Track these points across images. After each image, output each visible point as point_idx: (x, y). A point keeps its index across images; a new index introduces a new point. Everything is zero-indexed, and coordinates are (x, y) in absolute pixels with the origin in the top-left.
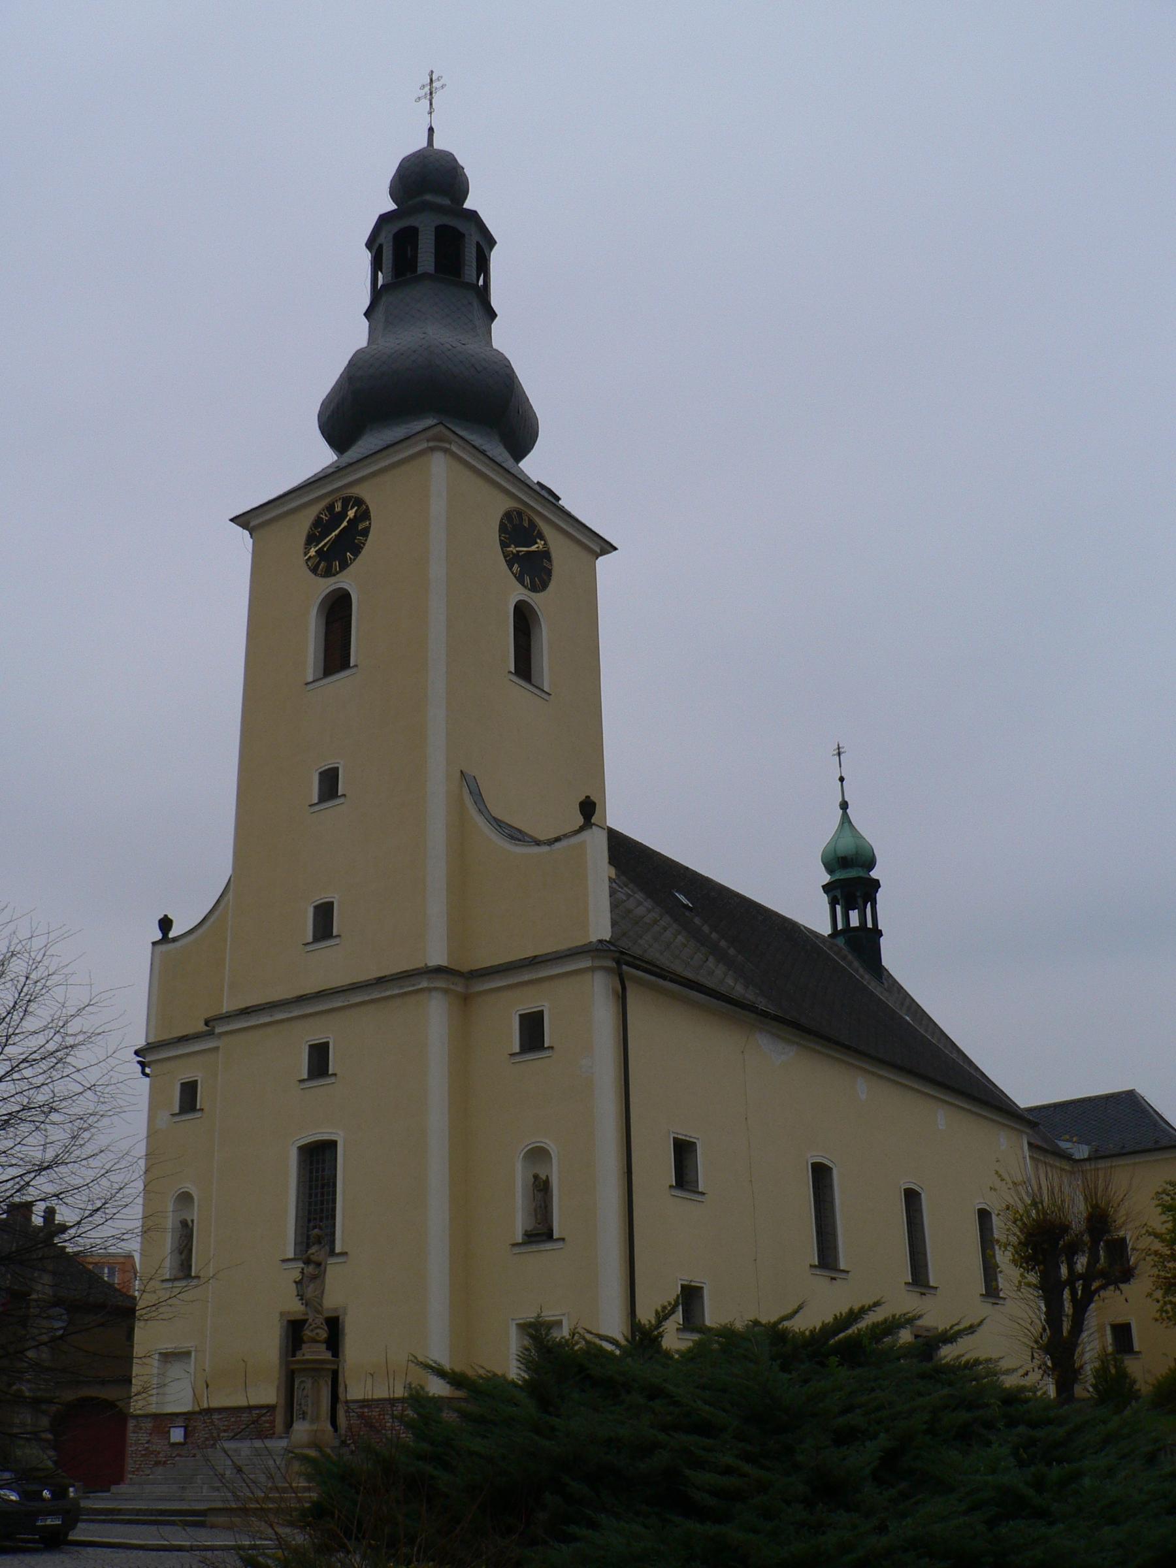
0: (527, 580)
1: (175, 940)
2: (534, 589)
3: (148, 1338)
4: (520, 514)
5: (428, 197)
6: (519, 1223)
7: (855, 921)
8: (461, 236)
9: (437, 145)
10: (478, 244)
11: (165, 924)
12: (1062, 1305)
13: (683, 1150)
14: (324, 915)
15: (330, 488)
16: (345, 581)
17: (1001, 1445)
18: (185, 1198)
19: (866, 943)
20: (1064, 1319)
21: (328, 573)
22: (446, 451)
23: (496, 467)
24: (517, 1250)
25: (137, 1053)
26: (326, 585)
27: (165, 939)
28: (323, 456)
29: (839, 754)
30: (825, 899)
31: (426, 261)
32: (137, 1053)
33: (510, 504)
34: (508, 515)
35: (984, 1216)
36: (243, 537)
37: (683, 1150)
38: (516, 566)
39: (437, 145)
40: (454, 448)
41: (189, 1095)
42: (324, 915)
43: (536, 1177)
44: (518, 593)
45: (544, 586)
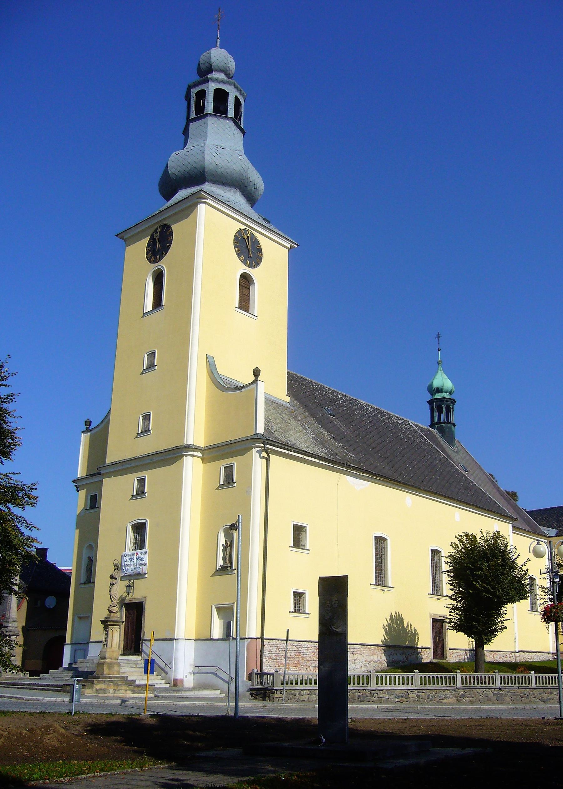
0: (248, 262)
2: (252, 266)
4: (246, 231)
8: (227, 94)
13: (298, 530)
15: (155, 222)
16: (164, 264)
20: (562, 630)
21: (155, 262)
22: (205, 203)
23: (157, 216)
25: (73, 481)
29: (439, 337)
31: (209, 107)
32: (73, 481)
34: (239, 232)
35: (435, 553)
37: (298, 530)
38: (242, 256)
40: (209, 201)
45: (258, 264)
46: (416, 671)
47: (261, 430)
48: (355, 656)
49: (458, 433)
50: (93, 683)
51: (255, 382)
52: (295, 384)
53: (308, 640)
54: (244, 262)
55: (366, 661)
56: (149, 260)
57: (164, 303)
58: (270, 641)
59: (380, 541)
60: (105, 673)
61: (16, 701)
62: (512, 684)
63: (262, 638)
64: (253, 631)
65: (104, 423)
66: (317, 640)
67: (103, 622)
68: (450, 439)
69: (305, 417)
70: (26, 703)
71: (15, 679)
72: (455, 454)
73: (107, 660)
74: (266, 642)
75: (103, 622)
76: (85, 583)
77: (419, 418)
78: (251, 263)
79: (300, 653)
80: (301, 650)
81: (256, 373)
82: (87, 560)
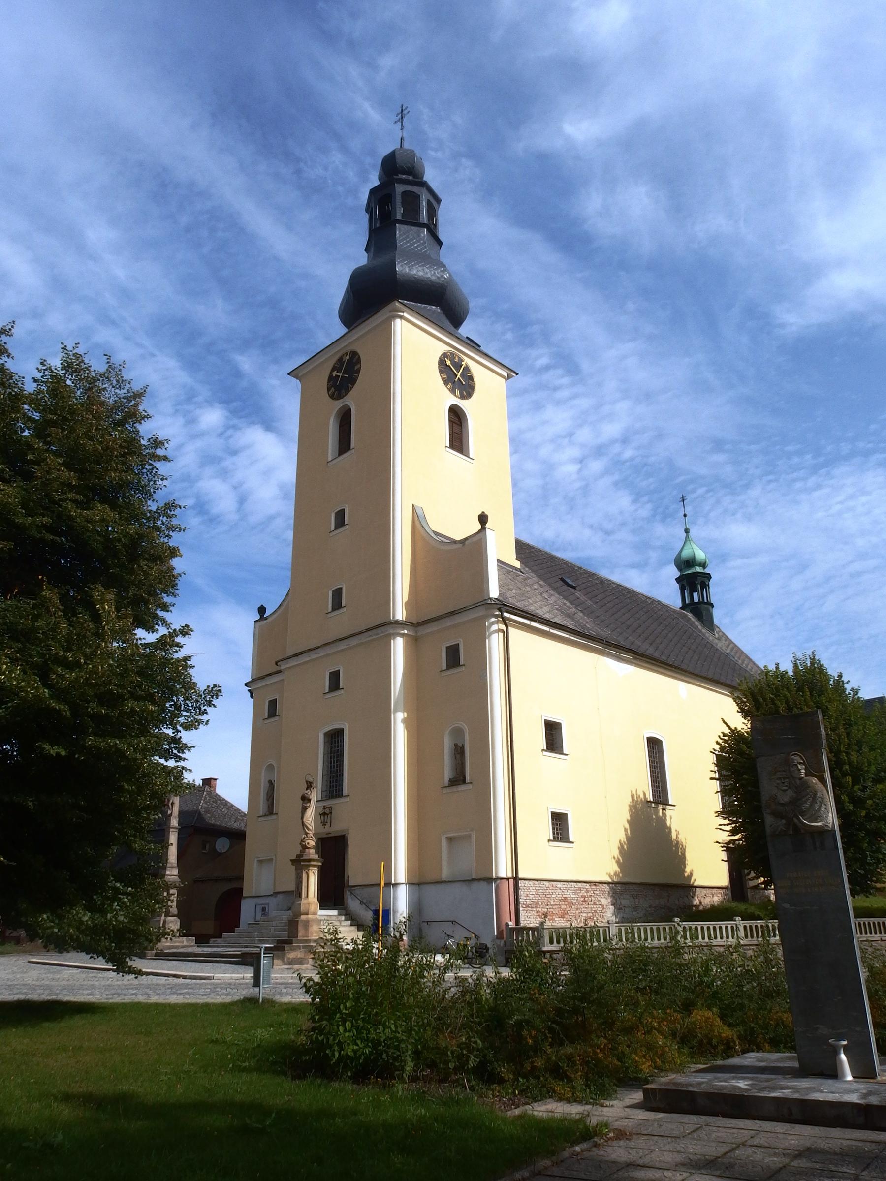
0: (458, 392)
1: (266, 618)
2: (462, 397)
3: (252, 849)
5: (400, 176)
6: (448, 774)
7: (696, 600)
9: (406, 146)
10: (429, 202)
11: (262, 610)
12: (179, 840)
14: (338, 594)
16: (350, 400)
17: (353, 1050)
18: (271, 767)
19: (701, 610)
22: (401, 317)
24: (445, 791)
25: (246, 685)
26: (338, 404)
27: (262, 618)
28: (340, 330)
29: (683, 501)
30: (677, 586)
31: (399, 211)
32: (246, 685)
33: (447, 348)
34: (445, 355)
36: (296, 383)
39: (406, 146)
40: (406, 315)
41: (273, 709)
42: (338, 594)
43: (456, 745)
44: (453, 400)
46: (737, 918)
47: (494, 592)
48: (637, 900)
49: (719, 616)
50: (284, 950)
51: (483, 528)
52: (523, 549)
53: (575, 879)
54: (453, 391)
55: (650, 907)
56: (332, 397)
57: (352, 446)
58: (527, 882)
59: (654, 745)
60: (300, 934)
61: (176, 980)
62: (871, 933)
63: (516, 879)
64: (503, 869)
65: (282, 608)
66: (726, 859)
67: (293, 861)
68: (708, 622)
69: (541, 586)
70: (188, 984)
71: (177, 947)
72: (716, 641)
73: (310, 916)
74: (521, 884)
75: (293, 861)
76: (265, 815)
77: (669, 594)
78: (461, 393)
79: (566, 898)
80: (568, 894)
81: (483, 519)
82: (268, 785)
